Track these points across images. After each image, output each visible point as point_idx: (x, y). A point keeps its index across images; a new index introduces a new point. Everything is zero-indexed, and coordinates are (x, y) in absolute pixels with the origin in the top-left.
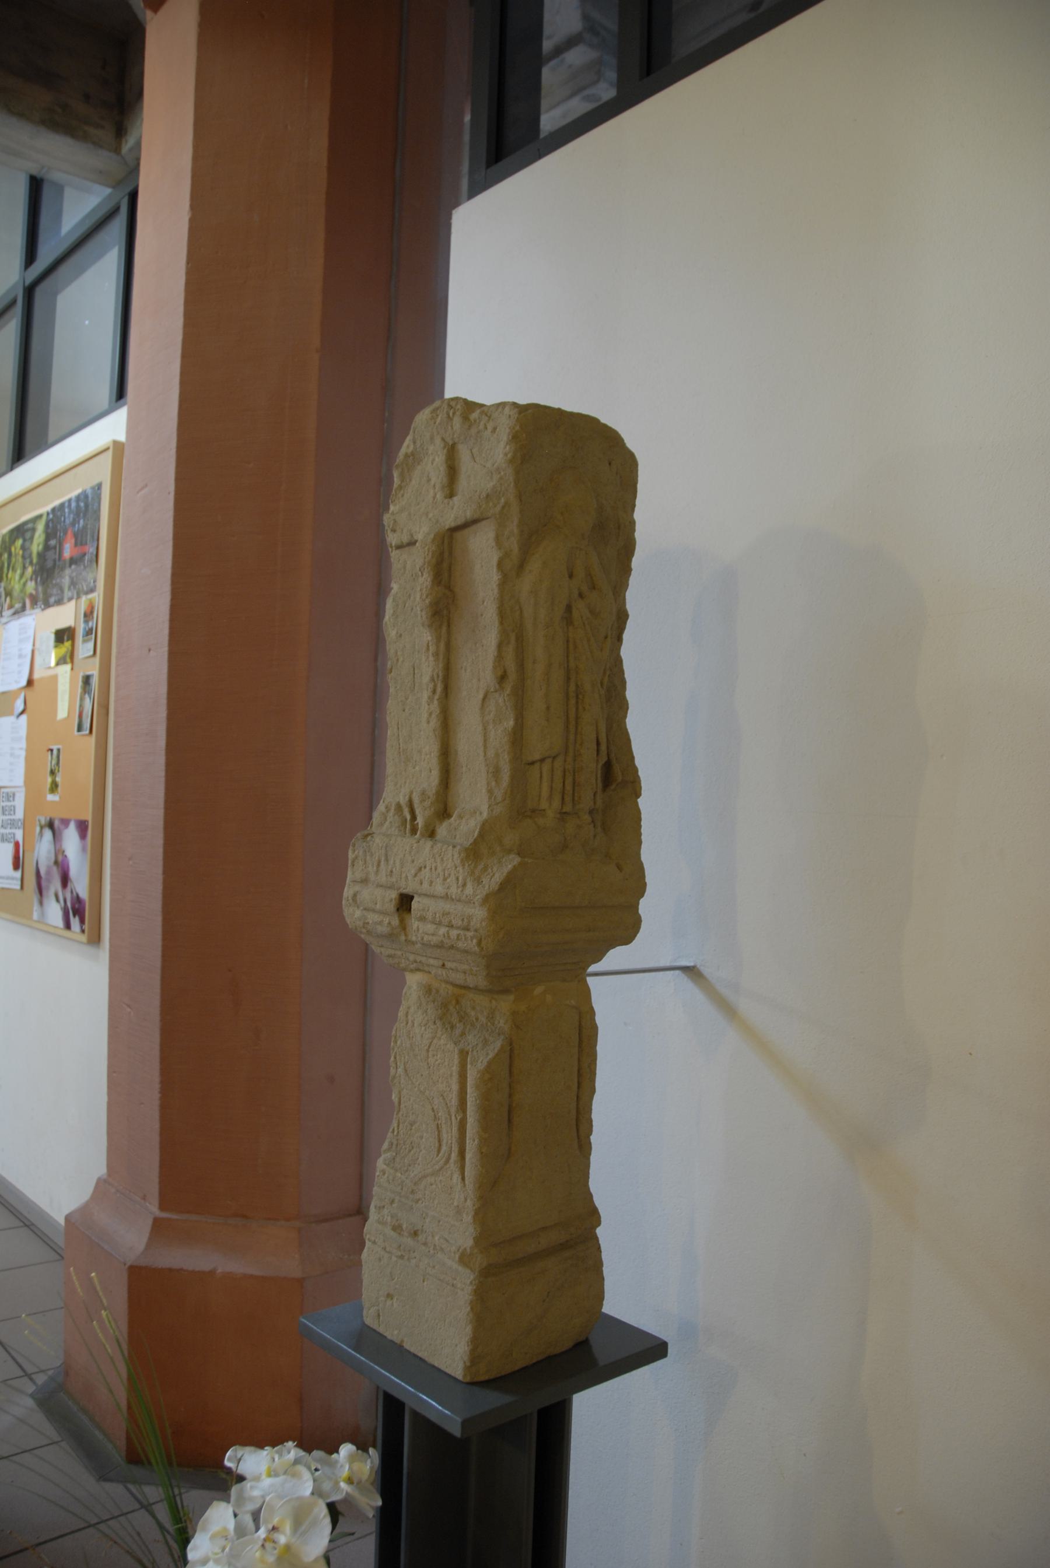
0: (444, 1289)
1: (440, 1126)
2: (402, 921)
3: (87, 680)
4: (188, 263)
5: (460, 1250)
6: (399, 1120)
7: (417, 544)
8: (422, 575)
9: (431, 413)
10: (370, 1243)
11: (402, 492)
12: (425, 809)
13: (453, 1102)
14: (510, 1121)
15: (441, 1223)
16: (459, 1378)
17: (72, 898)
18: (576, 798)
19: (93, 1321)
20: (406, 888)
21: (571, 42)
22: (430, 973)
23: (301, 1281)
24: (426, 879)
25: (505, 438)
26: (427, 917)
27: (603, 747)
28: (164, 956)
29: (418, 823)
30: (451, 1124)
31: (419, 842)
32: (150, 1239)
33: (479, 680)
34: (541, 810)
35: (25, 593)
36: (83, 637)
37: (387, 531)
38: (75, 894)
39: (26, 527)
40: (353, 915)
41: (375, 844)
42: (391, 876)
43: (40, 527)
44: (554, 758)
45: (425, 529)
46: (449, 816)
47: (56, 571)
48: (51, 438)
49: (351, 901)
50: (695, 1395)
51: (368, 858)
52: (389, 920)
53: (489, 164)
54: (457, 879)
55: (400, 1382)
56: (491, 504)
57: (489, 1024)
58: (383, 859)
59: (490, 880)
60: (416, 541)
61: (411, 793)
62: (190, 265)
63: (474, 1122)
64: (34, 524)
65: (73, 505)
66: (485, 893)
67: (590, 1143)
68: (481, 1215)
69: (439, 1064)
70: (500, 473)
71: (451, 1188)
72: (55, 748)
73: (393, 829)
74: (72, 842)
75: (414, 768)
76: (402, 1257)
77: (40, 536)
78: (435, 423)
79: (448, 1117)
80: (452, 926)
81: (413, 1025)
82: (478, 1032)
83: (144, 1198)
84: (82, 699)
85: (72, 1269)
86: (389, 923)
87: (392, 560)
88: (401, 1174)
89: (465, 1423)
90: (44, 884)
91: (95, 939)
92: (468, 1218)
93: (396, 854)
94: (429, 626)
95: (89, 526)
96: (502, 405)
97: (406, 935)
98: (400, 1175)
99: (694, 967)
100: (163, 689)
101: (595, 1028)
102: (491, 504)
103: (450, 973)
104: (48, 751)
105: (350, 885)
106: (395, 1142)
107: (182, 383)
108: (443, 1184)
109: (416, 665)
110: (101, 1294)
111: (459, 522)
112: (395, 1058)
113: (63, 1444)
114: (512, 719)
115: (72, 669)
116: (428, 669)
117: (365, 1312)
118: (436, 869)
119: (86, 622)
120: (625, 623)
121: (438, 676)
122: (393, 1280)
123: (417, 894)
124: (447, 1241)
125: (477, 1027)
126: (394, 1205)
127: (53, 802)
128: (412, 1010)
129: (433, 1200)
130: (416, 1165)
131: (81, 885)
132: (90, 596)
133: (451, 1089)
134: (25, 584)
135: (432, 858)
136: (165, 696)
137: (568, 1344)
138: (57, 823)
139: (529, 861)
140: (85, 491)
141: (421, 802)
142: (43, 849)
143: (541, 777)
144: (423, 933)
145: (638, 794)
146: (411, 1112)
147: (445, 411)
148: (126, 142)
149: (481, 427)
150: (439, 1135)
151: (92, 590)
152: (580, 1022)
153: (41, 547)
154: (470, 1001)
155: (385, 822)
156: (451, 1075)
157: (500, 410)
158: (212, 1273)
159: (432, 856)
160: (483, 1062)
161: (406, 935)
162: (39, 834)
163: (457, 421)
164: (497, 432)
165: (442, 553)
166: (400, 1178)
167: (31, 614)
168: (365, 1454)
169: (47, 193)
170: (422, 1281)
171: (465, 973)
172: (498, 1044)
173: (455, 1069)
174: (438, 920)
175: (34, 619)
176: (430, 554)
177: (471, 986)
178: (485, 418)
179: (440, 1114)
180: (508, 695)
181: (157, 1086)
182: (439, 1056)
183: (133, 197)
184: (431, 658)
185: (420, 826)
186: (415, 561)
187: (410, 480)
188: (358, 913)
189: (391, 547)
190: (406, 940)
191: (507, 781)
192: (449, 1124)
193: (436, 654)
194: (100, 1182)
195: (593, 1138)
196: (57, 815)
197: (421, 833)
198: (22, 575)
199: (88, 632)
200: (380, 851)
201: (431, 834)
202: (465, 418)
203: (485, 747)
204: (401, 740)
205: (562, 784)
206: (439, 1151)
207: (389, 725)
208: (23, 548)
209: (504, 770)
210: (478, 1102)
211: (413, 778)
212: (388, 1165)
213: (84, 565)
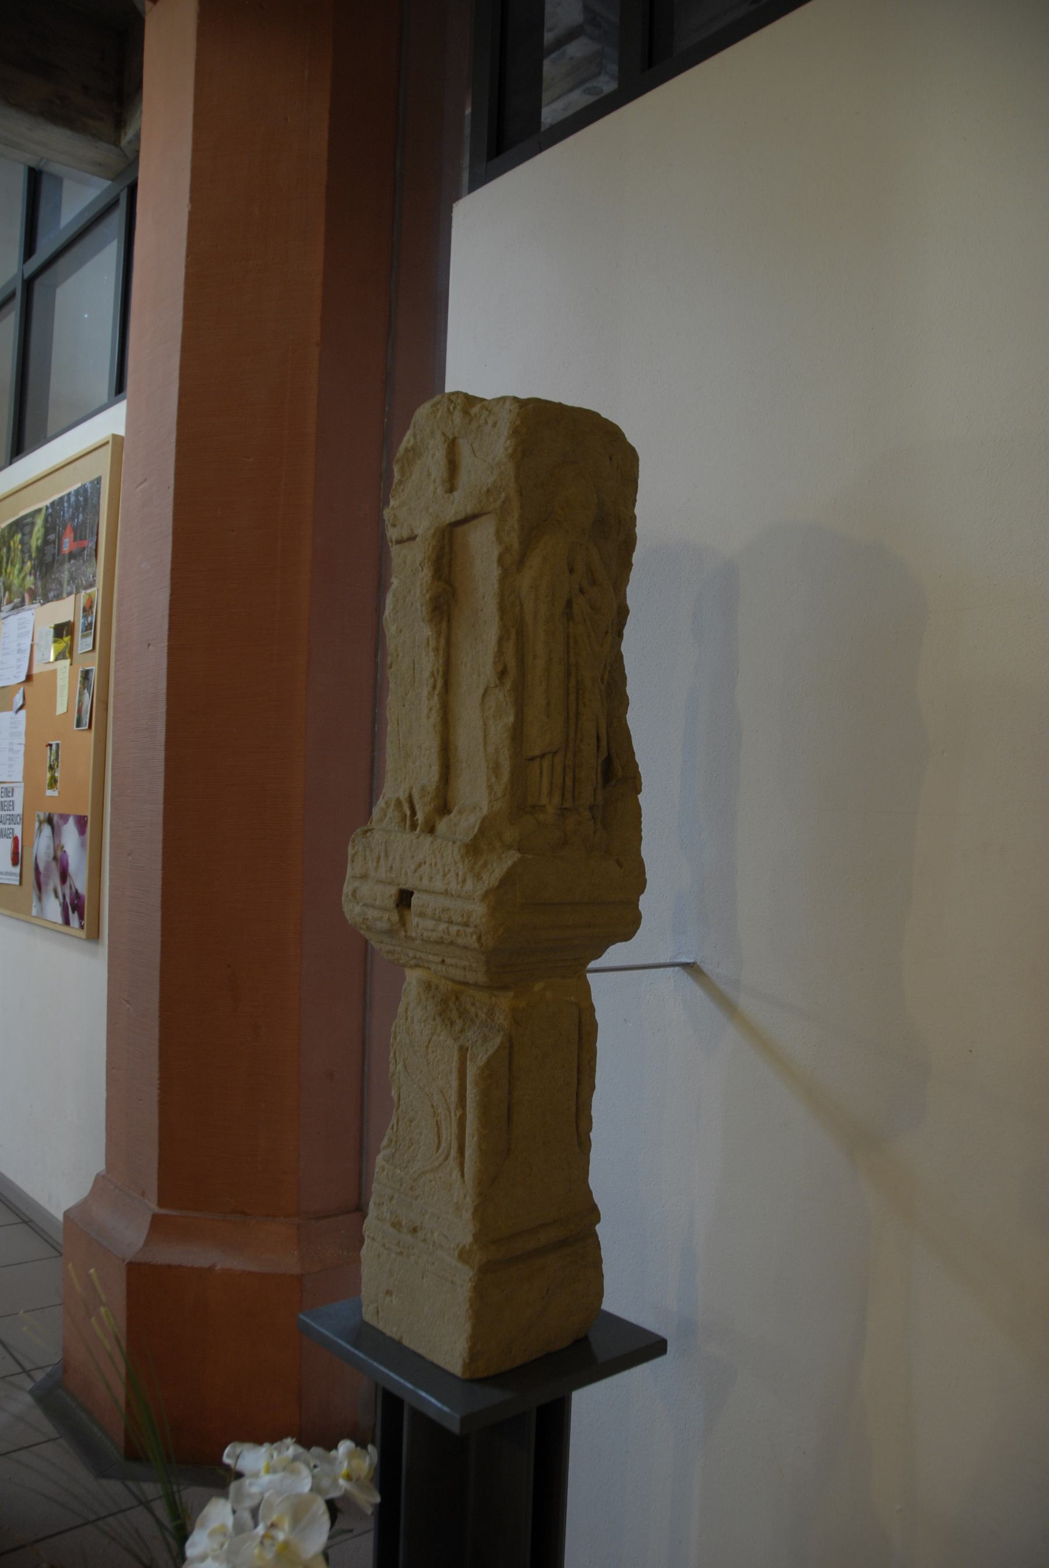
1: (439, 1123)
3: (86, 675)
4: (187, 256)
8: (422, 570)
11: (402, 487)
21: (572, 35)
22: (429, 968)
27: (604, 743)
29: (417, 819)
31: (419, 837)
32: (148, 1236)
33: (479, 676)
35: (24, 589)
36: (82, 632)
37: (387, 525)
40: (352, 911)
43: (40, 521)
44: (555, 753)
46: (449, 812)
47: (55, 566)
49: (350, 897)
51: (368, 853)
54: (457, 875)
57: (488, 1020)
58: (383, 855)
61: (411, 788)
62: (190, 257)
65: (73, 499)
68: (480, 1212)
69: (438, 1061)
70: (500, 468)
72: (54, 743)
73: (393, 825)
75: (414, 764)
76: (401, 1253)
77: (39, 530)
78: (435, 417)
80: (452, 922)
81: (413, 1022)
84: (81, 694)
86: (389, 919)
88: (401, 1170)
89: (464, 1421)
90: (42, 879)
91: (94, 935)
92: (467, 1215)
96: (503, 399)
97: (406, 931)
98: (399, 1171)
99: (694, 963)
100: (163, 685)
101: (594, 1025)
102: (491, 499)
104: (47, 746)
106: (394, 1139)
111: (460, 517)
112: (395, 1054)
114: (512, 715)
115: (71, 664)
116: (428, 664)
117: (364, 1310)
118: (436, 865)
119: (85, 617)
120: (626, 619)
121: (438, 672)
126: (394, 1202)
131: (80, 881)
132: (89, 591)
134: (24, 579)
138: (56, 819)
141: (421, 798)
142: (42, 845)
143: (541, 773)
145: (638, 790)
147: (445, 406)
148: (126, 134)
149: (482, 421)
153: (40, 542)
156: (451, 1072)
157: (501, 403)
158: (211, 1269)
161: (406, 931)
163: (458, 416)
167: (30, 609)
169: (46, 186)
171: (465, 969)
172: (498, 1041)
173: (455, 1065)
174: (438, 916)
176: (431, 548)
177: (470, 982)
178: (485, 413)
180: (508, 690)
182: (438, 1052)
184: (431, 654)
185: (419, 822)
186: (414, 555)
187: (411, 475)
188: (358, 909)
189: (392, 542)
190: (405, 936)
193: (436, 650)
194: (99, 1179)
196: (56, 811)
198: (21, 570)
199: (88, 627)
201: (431, 830)
202: (466, 412)
206: (438, 1148)
208: (22, 542)
210: (477, 1098)
212: (387, 1161)
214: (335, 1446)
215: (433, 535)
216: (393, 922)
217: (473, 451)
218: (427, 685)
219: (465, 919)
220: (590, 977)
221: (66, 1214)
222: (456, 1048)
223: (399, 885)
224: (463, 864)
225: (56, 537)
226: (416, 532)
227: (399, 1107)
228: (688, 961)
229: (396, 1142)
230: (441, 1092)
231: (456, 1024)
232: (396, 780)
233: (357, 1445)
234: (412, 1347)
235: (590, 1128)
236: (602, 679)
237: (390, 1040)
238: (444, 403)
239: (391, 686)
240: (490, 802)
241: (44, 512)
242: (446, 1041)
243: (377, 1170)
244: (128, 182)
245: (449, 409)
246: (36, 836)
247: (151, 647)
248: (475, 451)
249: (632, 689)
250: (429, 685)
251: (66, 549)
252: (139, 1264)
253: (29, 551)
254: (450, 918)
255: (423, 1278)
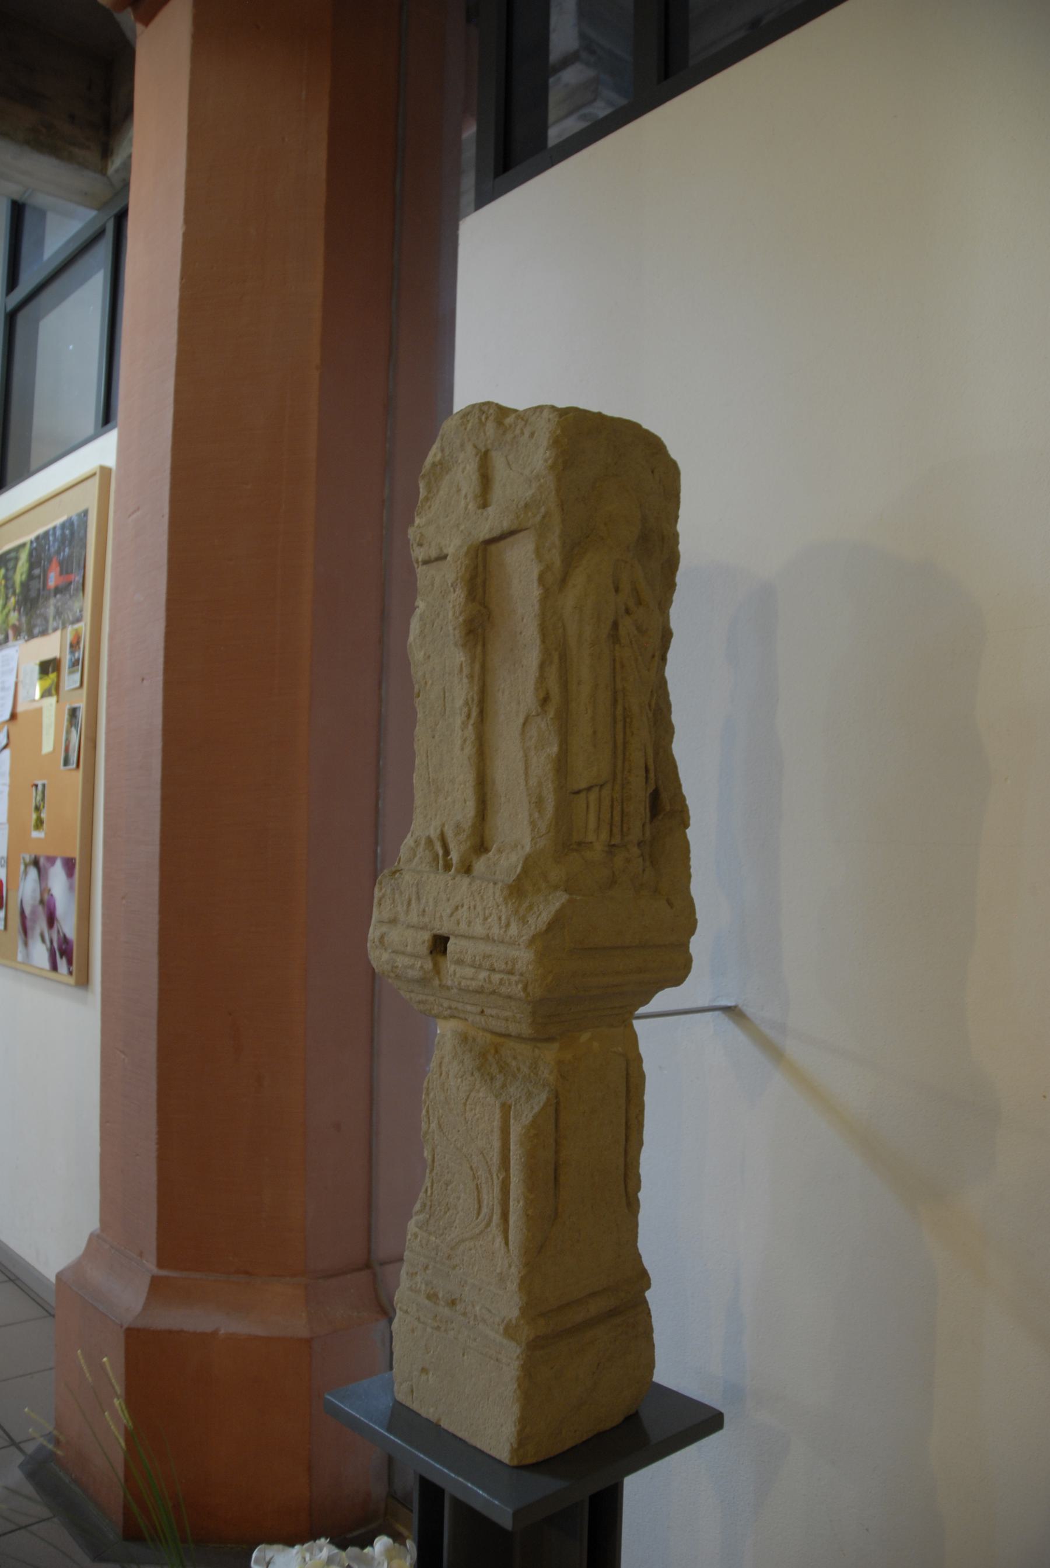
0: (487, 1364)
1: (479, 1187)
2: (436, 965)
3: (73, 713)
4: (182, 278)
5: (505, 1322)
6: (432, 1179)
7: (448, 558)
8: (454, 591)
9: (461, 418)
10: (402, 1313)
11: (428, 504)
12: (461, 843)
13: (495, 1160)
14: (556, 1179)
15: (482, 1291)
16: (505, 1462)
17: (59, 939)
18: (625, 829)
19: (104, 1412)
20: (441, 929)
21: (567, 61)
22: (466, 1020)
23: (308, 1342)
24: (464, 919)
25: (545, 443)
26: (465, 960)
27: (652, 775)
28: (160, 1000)
29: (451, 859)
30: (493, 1184)
31: (454, 879)
32: (147, 1299)
33: (519, 703)
34: (588, 843)
35: (8, 625)
36: (69, 668)
37: (412, 545)
38: (61, 934)
39: (9, 557)
40: (379, 958)
41: (404, 882)
42: (423, 915)
43: (24, 556)
44: (602, 786)
45: (457, 541)
46: (487, 850)
47: (41, 601)
48: (33, 467)
49: (378, 943)
50: (743, 1464)
51: (397, 896)
52: (422, 963)
53: (497, 175)
54: (500, 918)
55: (441, 1468)
56: (530, 514)
57: (532, 1074)
58: (414, 897)
59: (537, 919)
60: (445, 557)
61: (443, 825)
62: (184, 280)
63: (519, 1182)
64: (17, 553)
65: (58, 532)
66: (531, 934)
67: (638, 1200)
68: (526, 1283)
69: (478, 1119)
70: (539, 480)
71: (493, 1253)
72: (40, 783)
73: (424, 865)
74: (58, 881)
75: (446, 799)
76: (438, 1328)
77: (23, 565)
78: (465, 429)
79: (489, 1176)
80: (494, 970)
81: (448, 1077)
82: (521, 1084)
83: (141, 1254)
84: (68, 732)
85: (79, 1351)
86: (422, 967)
87: (418, 576)
88: (436, 1238)
89: (516, 1515)
90: (29, 924)
91: (84, 981)
92: (513, 1286)
93: (428, 892)
94: (462, 646)
95: (75, 554)
96: (540, 409)
97: (440, 980)
98: (434, 1239)
99: (736, 1007)
100: (158, 720)
101: (642, 1076)
103: (490, 1020)
104: (32, 786)
105: (375, 926)
106: (429, 1203)
107: (177, 401)
108: (484, 1249)
109: (446, 687)
110: (113, 1381)
111: (496, 533)
112: (428, 1112)
113: (55, 1519)
114: (556, 745)
115: (58, 701)
116: (461, 692)
117: (396, 1388)
118: (475, 908)
119: (72, 652)
120: (669, 642)
121: (473, 700)
122: (428, 1353)
123: (452, 934)
124: (490, 1311)
125: (519, 1078)
126: (428, 1272)
127: (39, 840)
128: (446, 1060)
129: (473, 1267)
130: (453, 1229)
131: (68, 925)
132: (77, 626)
133: (491, 1146)
134: (7, 615)
135: (470, 896)
136: (160, 727)
137: (618, 1419)
138: (42, 861)
139: (578, 898)
140: (71, 519)
141: (456, 835)
142: (28, 888)
143: (588, 807)
144: (461, 977)
145: (686, 825)
146: (446, 1171)
147: (476, 416)
148: (113, 163)
149: (518, 431)
150: (478, 1196)
151: (78, 620)
152: (627, 1070)
153: (24, 577)
154: (510, 1050)
155: (414, 858)
156: (492, 1131)
157: (538, 413)
158: (214, 1334)
159: (470, 894)
160: (528, 1117)
161: (440, 980)
162: (23, 872)
163: (490, 427)
164: (534, 438)
165: (476, 567)
166: (435, 1242)
167: (14, 646)
168: (402, 1547)
170: (461, 1355)
171: (507, 1020)
172: (544, 1096)
173: (497, 1124)
174: (478, 963)
175: (17, 651)
176: (463, 569)
177: (513, 1034)
178: (521, 423)
179: (479, 1173)
180: (552, 719)
181: (154, 1137)
182: (477, 1110)
183: (121, 218)
184: (465, 680)
185: (454, 862)
186: (444, 576)
187: (438, 491)
188: (385, 956)
189: (417, 562)
190: (440, 985)
191: (551, 812)
192: (490, 1183)
193: (471, 677)
194: (93, 1238)
195: (641, 1195)
196: (42, 853)
197: (456, 869)
199: (75, 663)
200: (411, 889)
201: (467, 869)
202: (499, 423)
203: (526, 774)
204: (430, 769)
205: (610, 815)
206: (479, 1214)
207: (417, 753)
209: (548, 799)
210: (523, 1160)
211: (444, 810)
212: (420, 1228)
213: (70, 594)
214: (371, 1543)
215: (467, 553)
216: (426, 969)
217: (509, 464)
218: (461, 714)
219: (509, 967)
220: (637, 1024)
221: (59, 1276)
222: (498, 1105)
223: (433, 929)
224: (506, 907)
225: (41, 572)
226: (445, 551)
227: (433, 1169)
228: (729, 1004)
229: (431, 1207)
230: (482, 1153)
231: (496, 1079)
232: (425, 817)
233: (395, 1541)
234: (452, 1429)
235: (638, 1188)
236: (650, 706)
237: (422, 1097)
238: (475, 413)
239: (418, 716)
240: (532, 839)
241: (28, 546)
242: (486, 1098)
243: (409, 1237)
244: (116, 210)
245: (480, 419)
246: (22, 879)
247: (145, 682)
248: (511, 463)
249: (677, 718)
250: (463, 714)
251: (52, 583)
252: (138, 1330)
253: (13, 586)
254: (492, 965)
255: (463, 1355)
